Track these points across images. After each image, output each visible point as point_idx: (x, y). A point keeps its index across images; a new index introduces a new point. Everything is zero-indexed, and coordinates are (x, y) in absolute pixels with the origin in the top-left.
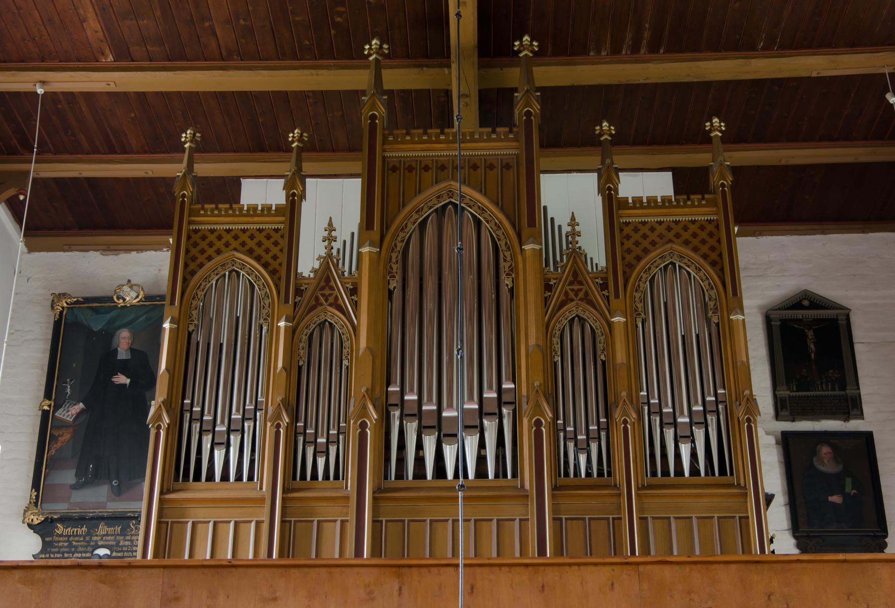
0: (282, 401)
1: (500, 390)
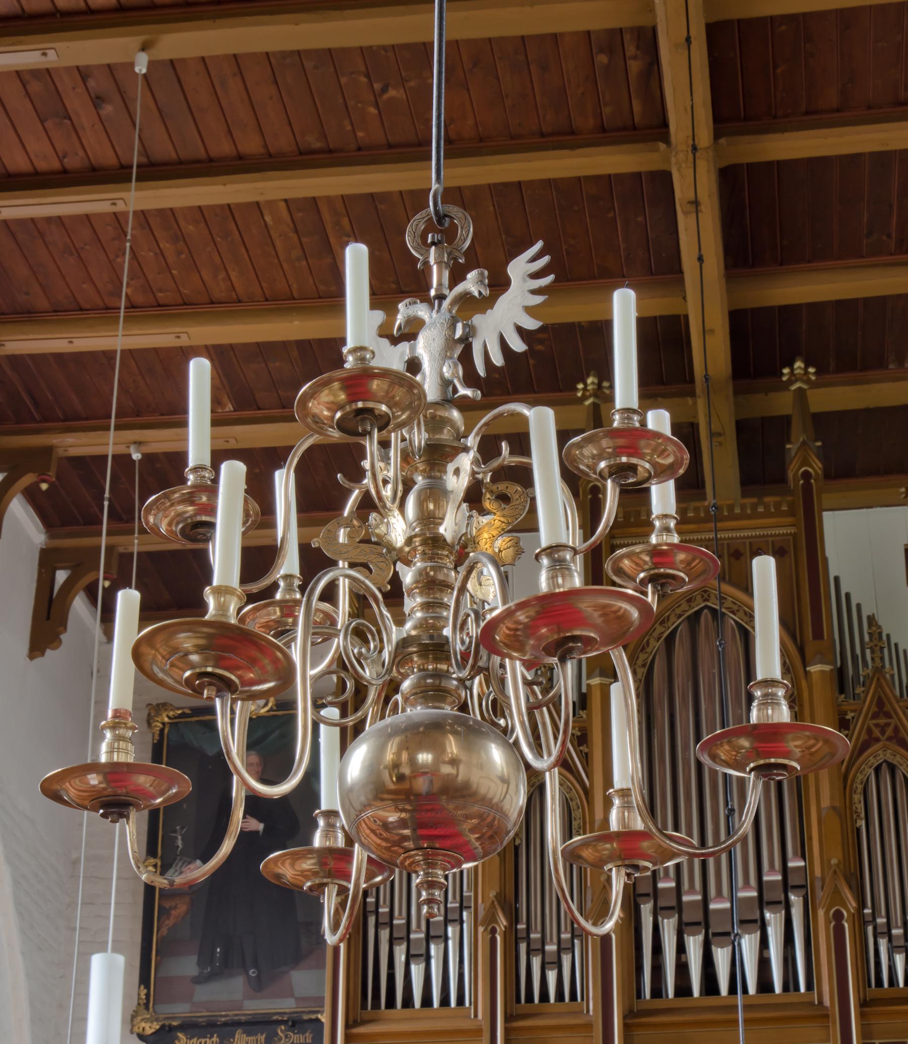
0: (496, 897)
1: (785, 870)
